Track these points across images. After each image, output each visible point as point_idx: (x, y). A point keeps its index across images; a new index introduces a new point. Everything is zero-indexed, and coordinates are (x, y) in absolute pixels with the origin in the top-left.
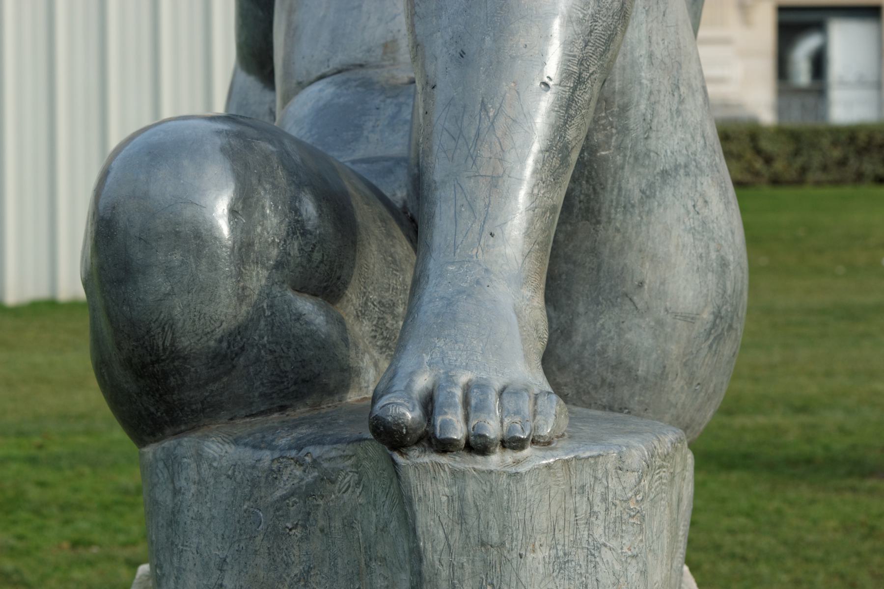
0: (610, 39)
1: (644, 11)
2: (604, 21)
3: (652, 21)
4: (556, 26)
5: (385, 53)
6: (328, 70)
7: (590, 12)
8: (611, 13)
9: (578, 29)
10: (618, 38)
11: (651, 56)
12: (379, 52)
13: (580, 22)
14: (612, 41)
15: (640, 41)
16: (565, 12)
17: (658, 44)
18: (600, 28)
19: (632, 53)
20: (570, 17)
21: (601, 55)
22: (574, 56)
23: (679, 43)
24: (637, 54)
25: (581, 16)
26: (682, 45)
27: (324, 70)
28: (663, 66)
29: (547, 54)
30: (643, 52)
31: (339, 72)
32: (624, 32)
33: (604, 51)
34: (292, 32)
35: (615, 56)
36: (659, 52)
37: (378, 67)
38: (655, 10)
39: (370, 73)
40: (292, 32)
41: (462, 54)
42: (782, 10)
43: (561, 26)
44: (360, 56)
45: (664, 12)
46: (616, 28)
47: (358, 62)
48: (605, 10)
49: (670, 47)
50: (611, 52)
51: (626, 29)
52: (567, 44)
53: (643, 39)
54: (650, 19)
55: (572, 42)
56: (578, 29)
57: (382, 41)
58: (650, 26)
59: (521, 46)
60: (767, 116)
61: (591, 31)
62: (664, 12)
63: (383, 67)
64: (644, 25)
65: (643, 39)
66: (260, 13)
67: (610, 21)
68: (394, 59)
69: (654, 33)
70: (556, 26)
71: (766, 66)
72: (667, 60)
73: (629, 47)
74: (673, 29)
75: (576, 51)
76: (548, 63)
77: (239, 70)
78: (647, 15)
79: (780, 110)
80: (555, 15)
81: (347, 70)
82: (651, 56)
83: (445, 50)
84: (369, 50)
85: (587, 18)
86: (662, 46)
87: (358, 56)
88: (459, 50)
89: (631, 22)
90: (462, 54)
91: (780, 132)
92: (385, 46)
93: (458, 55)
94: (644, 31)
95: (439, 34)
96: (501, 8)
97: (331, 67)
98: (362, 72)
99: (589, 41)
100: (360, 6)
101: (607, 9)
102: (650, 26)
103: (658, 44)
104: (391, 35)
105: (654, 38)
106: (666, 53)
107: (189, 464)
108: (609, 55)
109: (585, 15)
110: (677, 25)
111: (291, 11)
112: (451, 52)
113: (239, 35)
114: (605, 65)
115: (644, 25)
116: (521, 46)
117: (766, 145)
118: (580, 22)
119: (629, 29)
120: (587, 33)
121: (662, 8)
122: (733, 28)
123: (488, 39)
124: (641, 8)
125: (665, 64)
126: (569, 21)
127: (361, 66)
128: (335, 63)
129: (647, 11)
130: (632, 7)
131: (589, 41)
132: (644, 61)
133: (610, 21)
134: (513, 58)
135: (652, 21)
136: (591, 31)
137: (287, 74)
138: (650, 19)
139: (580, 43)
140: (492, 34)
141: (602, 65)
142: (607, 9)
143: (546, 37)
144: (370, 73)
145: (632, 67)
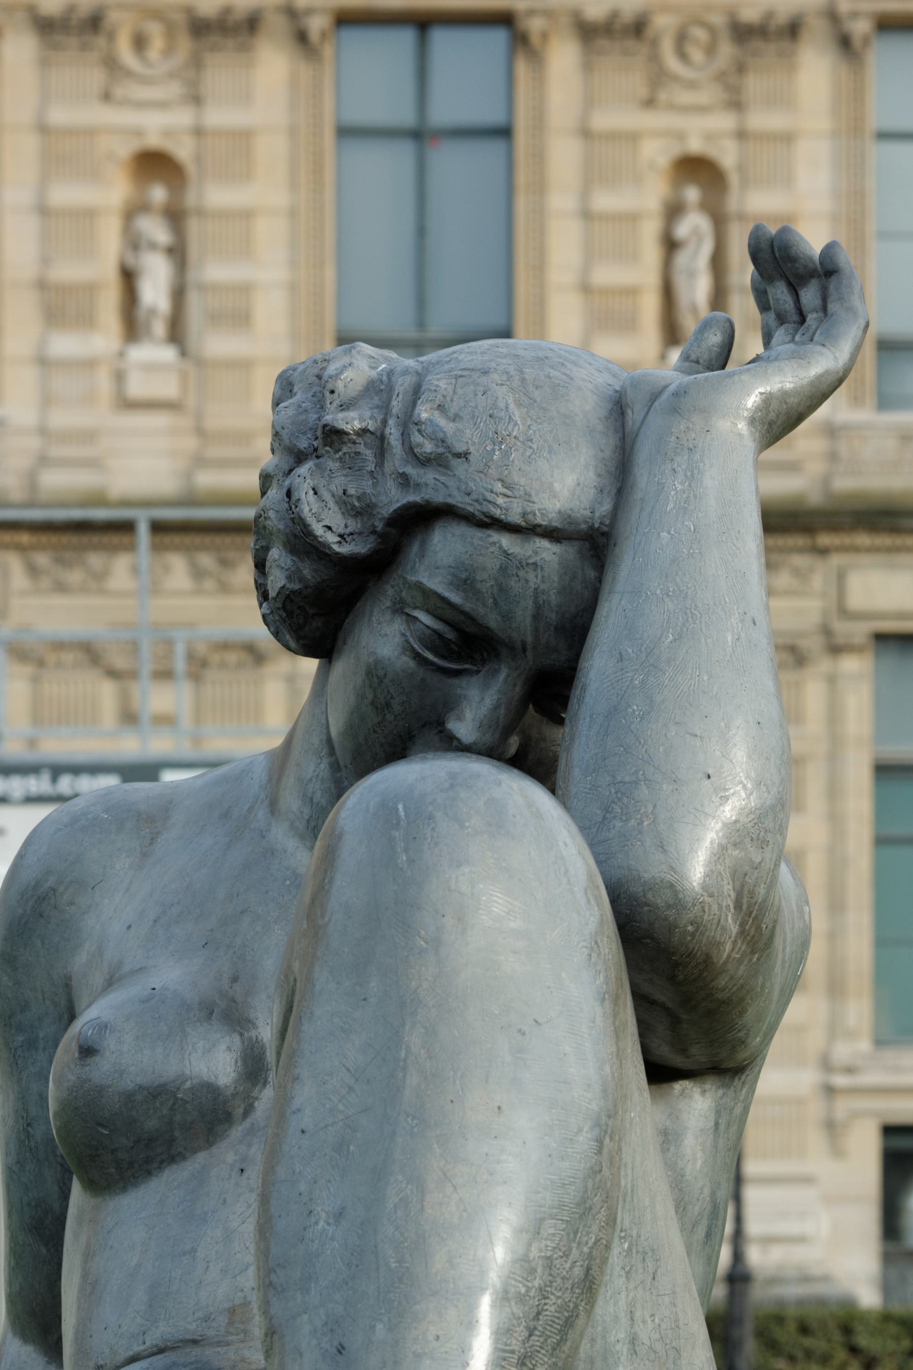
0: (569, 1323)
1: (623, 1273)
2: (558, 1298)
3: (636, 1288)
4: (484, 1308)
5: (231, 1323)
6: (143, 1347)
7: (536, 1283)
8: (569, 1285)
9: (518, 1310)
10: (580, 1322)
11: (633, 1340)
12: (223, 1320)
13: (521, 1299)
14: (571, 1326)
15: (616, 1319)
16: (498, 1284)
17: (644, 1322)
18: (552, 1309)
19: (604, 1337)
20: (506, 1292)
21: (554, 1349)
22: (513, 1352)
23: (677, 1320)
24: (612, 1339)
25: (523, 1290)
26: (681, 1323)
27: (137, 1348)
28: (652, 1356)
29: (470, 1349)
30: (621, 1335)
31: (161, 1351)
32: (589, 1312)
33: (559, 1343)
34: (91, 1288)
35: (576, 1349)
36: (646, 1334)
37: (219, 1344)
38: (641, 1270)
39: (207, 1353)
40: (91, 1288)
41: (341, 1349)
42: (890, 1131)
43: (493, 1306)
44: (192, 1327)
45: (654, 1274)
46: (576, 1306)
47: (189, 1337)
48: (559, 1280)
49: (664, 1326)
50: (569, 1343)
51: (592, 1307)
52: (501, 1334)
53: (622, 1315)
54: (632, 1286)
55: (508, 1330)
56: (518, 1310)
57: (227, 1305)
58: (631, 1295)
59: (431, 1338)
60: (869, 1298)
61: (538, 1313)
62: (654, 1274)
63: (228, 1344)
64: (623, 1295)
65: (622, 1315)
66: (44, 1251)
67: (567, 1296)
68: (245, 1332)
69: (638, 1305)
70: (484, 1308)
71: (868, 1217)
72: (658, 1346)
73: (600, 1328)
74: (667, 1299)
75: (516, 1345)
76: (472, 1363)
77: (10, 1335)
78: (628, 1278)
79: (887, 1288)
80: (483, 1290)
81: (173, 1348)
82: (633, 1340)
83: (314, 1342)
84: (206, 1319)
85: (532, 1294)
86: (650, 1325)
87: (191, 1327)
88: (336, 1343)
89: (602, 1290)
90: (341, 1349)
91: (886, 1318)
92: (232, 1311)
93: (335, 1351)
94: (622, 1303)
95: (305, 1317)
96: (400, 1280)
97: (148, 1344)
98: (195, 1353)
99: (535, 1328)
100: (194, 1250)
101: (563, 1278)
102: (631, 1295)
103: (644, 1322)
104: (240, 1294)
105: (638, 1314)
106: (657, 1336)
107: (380, 520)
108: (566, 1348)
109: (528, 1289)
110: (674, 1293)
111: (88, 1256)
112: (323, 1345)
113: (10, 1283)
114: (560, 1364)
115: (623, 1295)
116: (431, 1338)
117: (863, 1341)
118: (521, 1299)
119: (600, 1302)
120: (532, 1316)
121: (651, 1269)
122: (817, 1161)
123: (379, 1326)
124: (618, 1269)
125: (655, 1352)
126: (503, 1298)
127: (195, 1342)
128: (154, 1337)
129: (628, 1273)
130: (602, 1273)
131: (535, 1328)
132: (623, 1349)
133: (567, 1296)
134: (418, 1356)
135: (636, 1288)
136: (538, 1313)
137: (82, 1351)
138: (632, 1286)
139: (521, 1332)
140: (385, 1319)
141: (555, 1364)
142: (563, 1278)
143: (469, 1324)
144: (207, 1353)
145: (605, 1359)
